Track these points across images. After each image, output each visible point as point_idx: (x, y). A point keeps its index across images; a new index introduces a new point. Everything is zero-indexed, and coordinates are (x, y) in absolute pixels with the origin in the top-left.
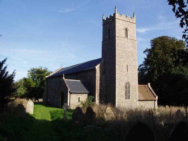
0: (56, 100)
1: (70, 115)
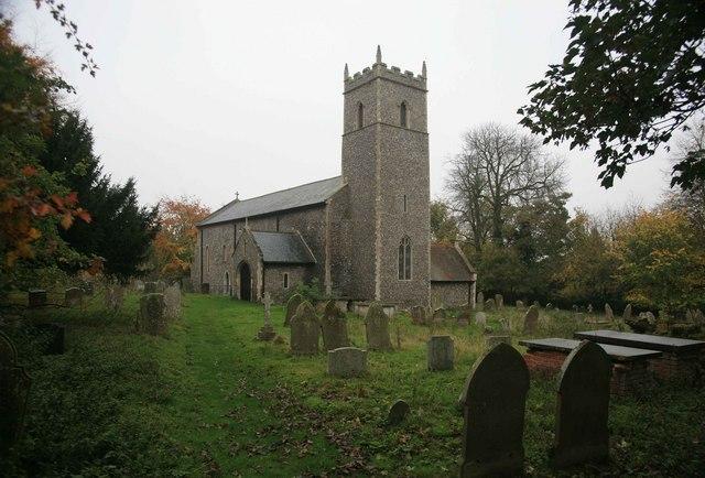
0: (225, 282)
1: (332, 280)
